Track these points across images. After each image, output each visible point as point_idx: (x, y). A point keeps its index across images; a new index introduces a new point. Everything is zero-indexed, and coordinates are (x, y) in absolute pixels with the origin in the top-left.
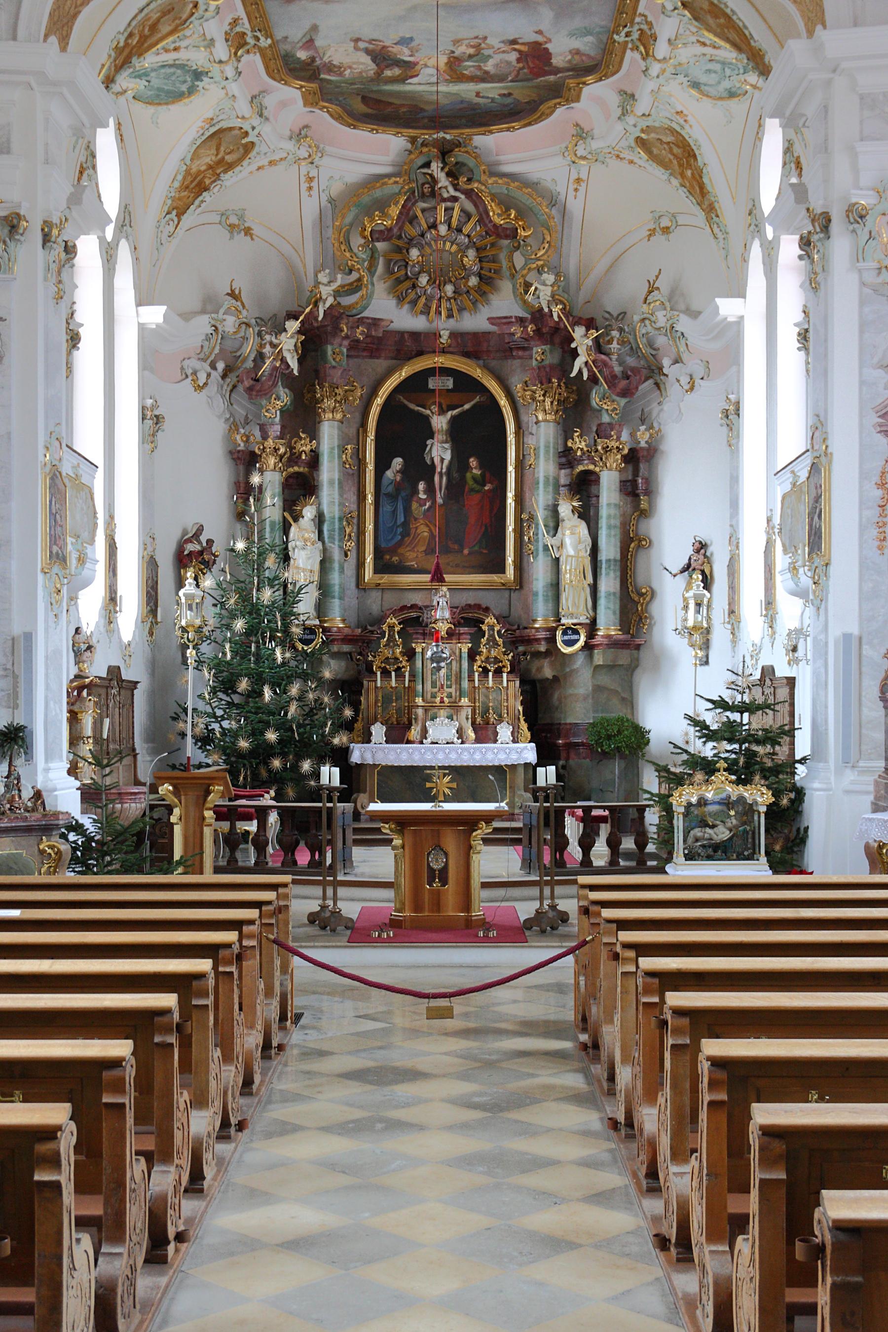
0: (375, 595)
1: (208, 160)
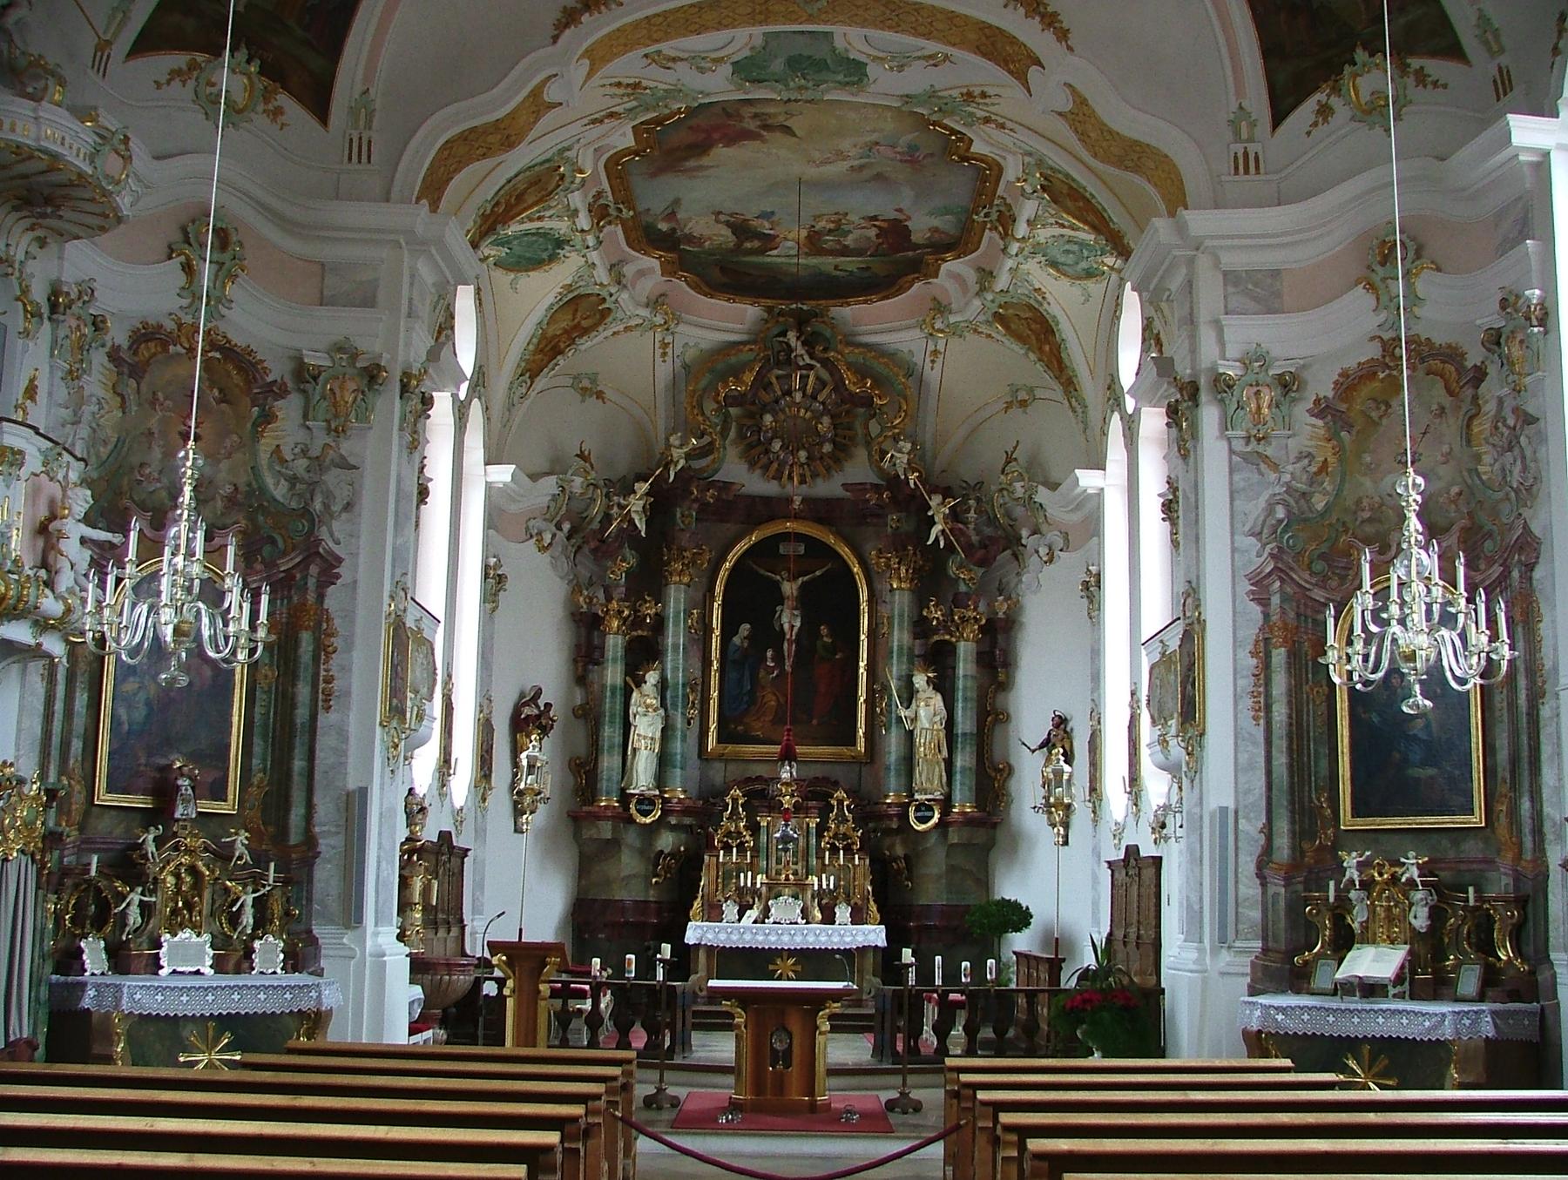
0: (719, 766)
1: (564, 325)
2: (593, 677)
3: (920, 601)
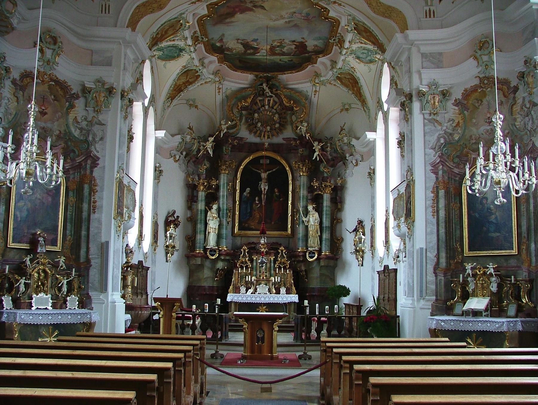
1: (183, 81)
2: (194, 207)
3: (310, 180)
